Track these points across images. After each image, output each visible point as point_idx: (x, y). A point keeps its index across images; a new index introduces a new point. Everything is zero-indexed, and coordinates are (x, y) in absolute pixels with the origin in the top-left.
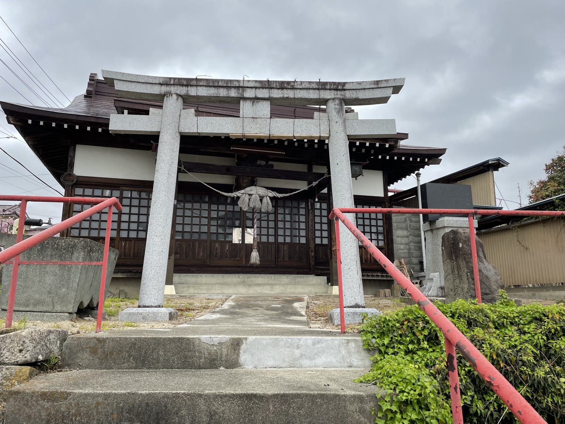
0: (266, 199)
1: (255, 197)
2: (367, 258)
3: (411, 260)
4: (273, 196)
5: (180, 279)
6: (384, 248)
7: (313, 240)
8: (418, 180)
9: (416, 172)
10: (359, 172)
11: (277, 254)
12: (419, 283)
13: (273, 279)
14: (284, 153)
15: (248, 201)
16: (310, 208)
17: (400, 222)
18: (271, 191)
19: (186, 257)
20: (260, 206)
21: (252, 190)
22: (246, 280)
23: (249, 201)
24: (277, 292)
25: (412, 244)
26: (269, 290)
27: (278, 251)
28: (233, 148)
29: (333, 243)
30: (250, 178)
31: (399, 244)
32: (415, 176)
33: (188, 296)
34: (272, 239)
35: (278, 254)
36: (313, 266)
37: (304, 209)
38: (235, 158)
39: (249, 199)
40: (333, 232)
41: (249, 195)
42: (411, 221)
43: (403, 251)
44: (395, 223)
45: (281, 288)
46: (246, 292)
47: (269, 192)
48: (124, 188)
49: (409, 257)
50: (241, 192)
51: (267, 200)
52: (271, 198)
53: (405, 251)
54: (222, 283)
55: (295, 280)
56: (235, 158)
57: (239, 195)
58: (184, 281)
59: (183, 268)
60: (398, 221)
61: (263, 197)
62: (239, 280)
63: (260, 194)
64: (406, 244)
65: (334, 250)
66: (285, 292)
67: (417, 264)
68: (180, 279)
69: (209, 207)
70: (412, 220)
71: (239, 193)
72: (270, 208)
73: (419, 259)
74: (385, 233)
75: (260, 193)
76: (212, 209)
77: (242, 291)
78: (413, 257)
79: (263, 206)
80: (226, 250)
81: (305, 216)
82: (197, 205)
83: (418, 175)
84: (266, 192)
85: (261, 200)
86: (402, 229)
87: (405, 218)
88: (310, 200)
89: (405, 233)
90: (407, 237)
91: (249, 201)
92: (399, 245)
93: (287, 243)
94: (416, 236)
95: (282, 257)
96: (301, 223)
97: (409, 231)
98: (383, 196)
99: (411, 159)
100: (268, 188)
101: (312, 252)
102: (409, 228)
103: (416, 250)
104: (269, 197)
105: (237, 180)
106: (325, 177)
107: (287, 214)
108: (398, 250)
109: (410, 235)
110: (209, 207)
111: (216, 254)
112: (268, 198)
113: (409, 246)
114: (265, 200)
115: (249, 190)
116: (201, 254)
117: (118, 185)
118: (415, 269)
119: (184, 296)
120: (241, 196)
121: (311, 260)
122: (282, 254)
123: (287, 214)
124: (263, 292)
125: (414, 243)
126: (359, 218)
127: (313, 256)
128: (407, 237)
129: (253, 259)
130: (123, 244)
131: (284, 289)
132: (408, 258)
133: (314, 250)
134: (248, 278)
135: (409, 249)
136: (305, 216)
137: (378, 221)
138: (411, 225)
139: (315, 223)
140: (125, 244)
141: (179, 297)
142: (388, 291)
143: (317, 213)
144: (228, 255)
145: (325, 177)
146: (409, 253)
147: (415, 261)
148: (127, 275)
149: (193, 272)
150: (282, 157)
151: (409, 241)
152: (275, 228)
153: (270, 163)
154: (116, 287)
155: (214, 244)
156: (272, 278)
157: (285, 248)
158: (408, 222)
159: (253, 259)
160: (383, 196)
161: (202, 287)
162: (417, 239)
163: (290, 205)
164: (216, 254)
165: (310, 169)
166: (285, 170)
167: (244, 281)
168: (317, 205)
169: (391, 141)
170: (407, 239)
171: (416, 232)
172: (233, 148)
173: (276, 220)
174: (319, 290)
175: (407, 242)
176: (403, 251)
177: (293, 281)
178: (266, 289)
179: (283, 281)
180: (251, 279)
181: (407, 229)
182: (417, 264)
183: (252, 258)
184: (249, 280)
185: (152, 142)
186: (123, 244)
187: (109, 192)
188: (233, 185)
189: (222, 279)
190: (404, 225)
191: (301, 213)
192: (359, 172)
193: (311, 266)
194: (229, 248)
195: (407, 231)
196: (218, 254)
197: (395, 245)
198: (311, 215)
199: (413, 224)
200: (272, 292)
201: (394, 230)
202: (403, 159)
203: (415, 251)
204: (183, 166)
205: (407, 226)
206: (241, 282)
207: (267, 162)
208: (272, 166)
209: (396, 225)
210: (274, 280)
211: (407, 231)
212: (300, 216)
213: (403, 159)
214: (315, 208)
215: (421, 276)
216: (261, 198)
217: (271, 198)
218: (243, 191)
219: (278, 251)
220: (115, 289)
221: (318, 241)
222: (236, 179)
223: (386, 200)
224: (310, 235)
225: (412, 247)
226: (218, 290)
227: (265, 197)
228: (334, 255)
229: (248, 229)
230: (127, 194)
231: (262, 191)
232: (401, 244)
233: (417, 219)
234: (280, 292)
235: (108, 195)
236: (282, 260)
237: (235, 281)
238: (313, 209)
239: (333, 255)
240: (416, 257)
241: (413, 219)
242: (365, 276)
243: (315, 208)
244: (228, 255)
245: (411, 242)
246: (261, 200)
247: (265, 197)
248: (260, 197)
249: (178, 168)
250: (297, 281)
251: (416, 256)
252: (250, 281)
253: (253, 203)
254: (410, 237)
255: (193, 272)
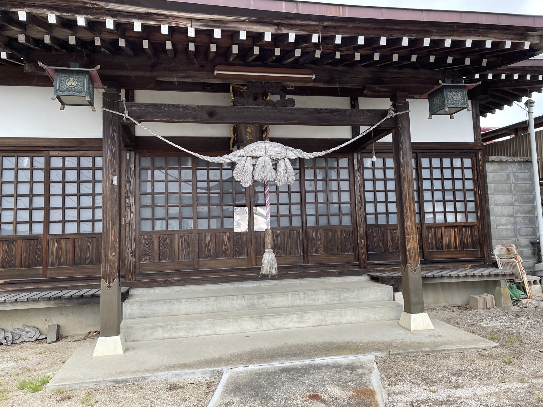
0: (283, 164)
1: (265, 162)
2: (450, 242)
3: (518, 240)
4: (296, 157)
5: (143, 309)
6: (476, 225)
7: (363, 219)
8: (529, 112)
9: (525, 99)
10: (462, 104)
11: (305, 245)
12: (538, 282)
13: (302, 297)
14: (314, 77)
15: (250, 168)
16: (356, 168)
17: (499, 181)
18: (292, 149)
19: (160, 260)
20: (274, 177)
21: (257, 150)
22: (256, 302)
23: (254, 169)
24: (311, 324)
25: (519, 215)
26: (295, 322)
27: (306, 240)
28: (219, 72)
29: (407, 237)
30: (257, 126)
31: (499, 216)
32: (524, 106)
33: (132, 380)
34: (38, 229)
35: (307, 246)
36: (365, 262)
37: (347, 171)
38: (229, 92)
39: (254, 165)
40: (407, 217)
41: (253, 158)
42: (517, 179)
43: (504, 227)
44: (492, 183)
45: (317, 317)
46: (257, 328)
47: (289, 149)
48: (51, 153)
49: (515, 236)
50: (239, 154)
51: (285, 166)
52: (293, 162)
53: (509, 227)
54: (216, 310)
55: (339, 296)
56: (229, 92)
57: (235, 159)
58: (149, 312)
59: (156, 279)
60: (497, 179)
61: (279, 160)
62: (244, 303)
63: (272, 155)
64: (511, 216)
65: (409, 249)
66: (324, 323)
67: (527, 246)
68: (143, 309)
69: (194, 174)
70: (518, 176)
71: (235, 156)
72: (293, 175)
73: (530, 237)
74: (478, 201)
75: (271, 153)
76: (198, 179)
77: (249, 328)
78: (521, 235)
79: (279, 177)
80: (224, 243)
81: (348, 181)
82: (173, 173)
83: (529, 104)
84: (283, 151)
85: (275, 166)
86: (502, 192)
87: (508, 175)
88: (355, 156)
89: (508, 198)
90: (512, 204)
91: (254, 169)
92: (499, 218)
93: (322, 227)
94: (525, 202)
95: (314, 250)
96: (342, 193)
97: (514, 195)
98: (473, 141)
99: (529, 77)
100: (287, 142)
101: (362, 238)
102: (515, 189)
103: (526, 224)
104: (289, 159)
105: (235, 130)
106: (389, 116)
107: (320, 180)
108: (497, 226)
109: (515, 201)
110: (194, 174)
111: (209, 250)
112: (287, 161)
113: (514, 219)
114: (281, 165)
115: (252, 149)
116: (185, 254)
117: (39, 149)
118: (525, 255)
119: (123, 381)
120: (239, 160)
121: (360, 251)
122: (314, 244)
123: (320, 180)
124: (286, 326)
125: (522, 213)
126: (435, 179)
127: (364, 246)
128: (512, 204)
129: (267, 266)
130: (56, 244)
131: (321, 318)
132: (514, 237)
133: (365, 235)
134: (259, 298)
135: (515, 223)
136: (348, 181)
137: (466, 182)
138: (516, 185)
139: (365, 191)
140: (59, 245)
141: (113, 384)
142: (489, 298)
143: (368, 174)
144: (229, 251)
145: (389, 116)
146: (514, 229)
147: (524, 241)
148: (55, 304)
149: (172, 283)
150: (310, 85)
151: (514, 210)
152: (301, 204)
153: (288, 97)
154: (44, 319)
155: (205, 236)
156: (300, 296)
157: (319, 235)
158: (513, 180)
159: (267, 266)
160: (473, 141)
161: (178, 327)
162: (527, 207)
163: (324, 165)
164: (209, 250)
165: (354, 104)
166: (316, 109)
167: (253, 305)
168: (367, 163)
169: (533, 36)
170: (511, 207)
171: (526, 196)
172: (219, 72)
173: (302, 179)
174: (381, 315)
175: (512, 213)
176: (504, 227)
177: (336, 298)
178: (291, 321)
179: (318, 300)
180: (266, 300)
181: (510, 192)
182: (527, 246)
183: (264, 266)
184: (261, 302)
185: (40, 64)
186: (56, 244)
187: (28, 161)
188: (230, 138)
189: (215, 303)
190: (505, 186)
191: (342, 177)
192: (462, 104)
193: (362, 261)
194: (229, 239)
195: (511, 195)
196: (212, 250)
197: (492, 219)
198: (358, 179)
199: (519, 183)
200: (301, 325)
201: (491, 194)
202: (516, 77)
203: (525, 226)
204: (126, 112)
205: (511, 187)
206: (248, 307)
207: (282, 97)
208: (293, 102)
209: (494, 186)
210: (304, 299)
211: (511, 195)
212: (341, 182)
213: (516, 77)
214: (365, 167)
215: (539, 270)
216: (274, 162)
217: (293, 162)
218: (241, 152)
219: (306, 240)
220: (44, 321)
221: (371, 220)
222: (233, 128)
223: (477, 148)
224: (359, 212)
225: (518, 219)
226: (206, 329)
227: (282, 160)
228: (410, 258)
229: (258, 208)
230: (56, 162)
231: (276, 149)
232: (503, 216)
233: (527, 175)
234: (315, 325)
235: (27, 165)
236: (314, 254)
237: (237, 306)
238: (362, 168)
239: (409, 259)
240: (524, 236)
241: (520, 174)
242: (454, 278)
243: (365, 167)
244: (229, 251)
245: (518, 211)
246: (275, 166)
247: (282, 160)
248: (273, 160)
249: (104, 112)
250: (342, 297)
251: (525, 234)
252: (263, 303)
253: (261, 173)
254: (517, 204)
255: (172, 283)
